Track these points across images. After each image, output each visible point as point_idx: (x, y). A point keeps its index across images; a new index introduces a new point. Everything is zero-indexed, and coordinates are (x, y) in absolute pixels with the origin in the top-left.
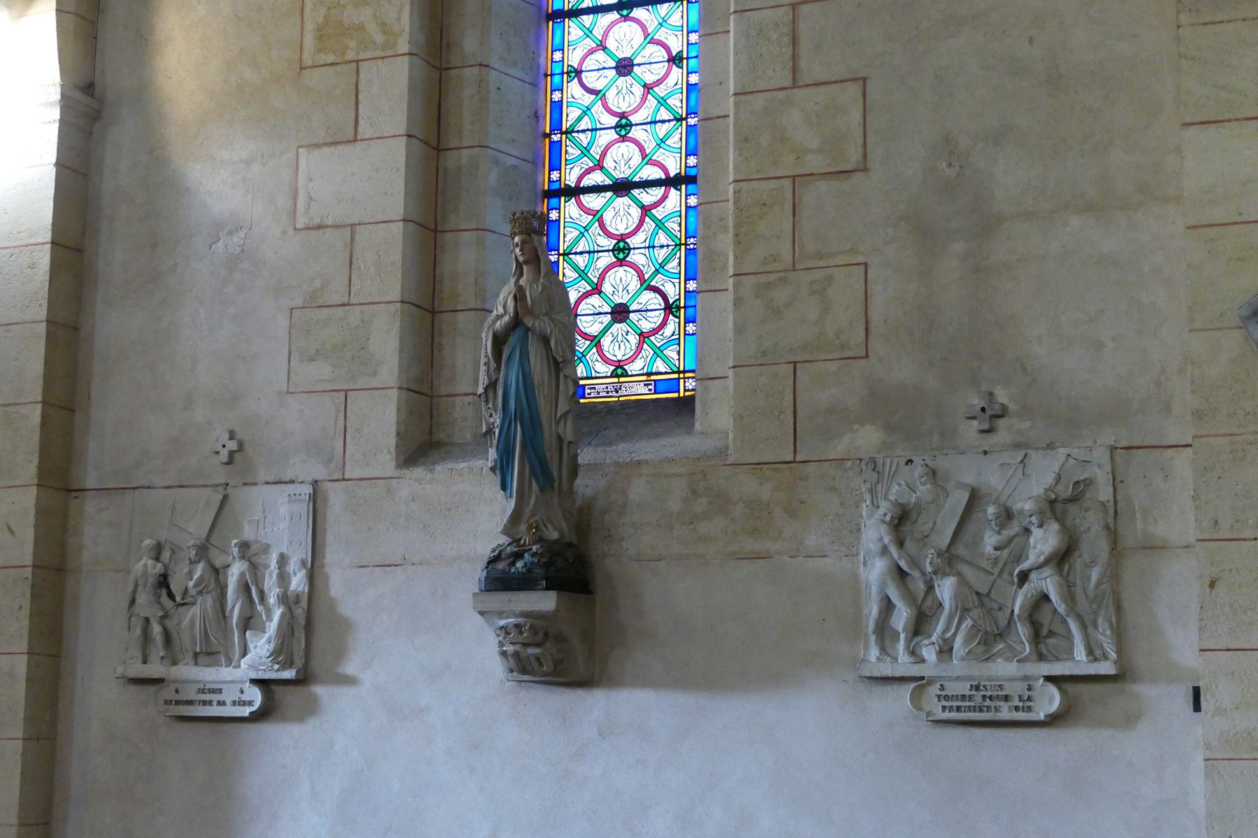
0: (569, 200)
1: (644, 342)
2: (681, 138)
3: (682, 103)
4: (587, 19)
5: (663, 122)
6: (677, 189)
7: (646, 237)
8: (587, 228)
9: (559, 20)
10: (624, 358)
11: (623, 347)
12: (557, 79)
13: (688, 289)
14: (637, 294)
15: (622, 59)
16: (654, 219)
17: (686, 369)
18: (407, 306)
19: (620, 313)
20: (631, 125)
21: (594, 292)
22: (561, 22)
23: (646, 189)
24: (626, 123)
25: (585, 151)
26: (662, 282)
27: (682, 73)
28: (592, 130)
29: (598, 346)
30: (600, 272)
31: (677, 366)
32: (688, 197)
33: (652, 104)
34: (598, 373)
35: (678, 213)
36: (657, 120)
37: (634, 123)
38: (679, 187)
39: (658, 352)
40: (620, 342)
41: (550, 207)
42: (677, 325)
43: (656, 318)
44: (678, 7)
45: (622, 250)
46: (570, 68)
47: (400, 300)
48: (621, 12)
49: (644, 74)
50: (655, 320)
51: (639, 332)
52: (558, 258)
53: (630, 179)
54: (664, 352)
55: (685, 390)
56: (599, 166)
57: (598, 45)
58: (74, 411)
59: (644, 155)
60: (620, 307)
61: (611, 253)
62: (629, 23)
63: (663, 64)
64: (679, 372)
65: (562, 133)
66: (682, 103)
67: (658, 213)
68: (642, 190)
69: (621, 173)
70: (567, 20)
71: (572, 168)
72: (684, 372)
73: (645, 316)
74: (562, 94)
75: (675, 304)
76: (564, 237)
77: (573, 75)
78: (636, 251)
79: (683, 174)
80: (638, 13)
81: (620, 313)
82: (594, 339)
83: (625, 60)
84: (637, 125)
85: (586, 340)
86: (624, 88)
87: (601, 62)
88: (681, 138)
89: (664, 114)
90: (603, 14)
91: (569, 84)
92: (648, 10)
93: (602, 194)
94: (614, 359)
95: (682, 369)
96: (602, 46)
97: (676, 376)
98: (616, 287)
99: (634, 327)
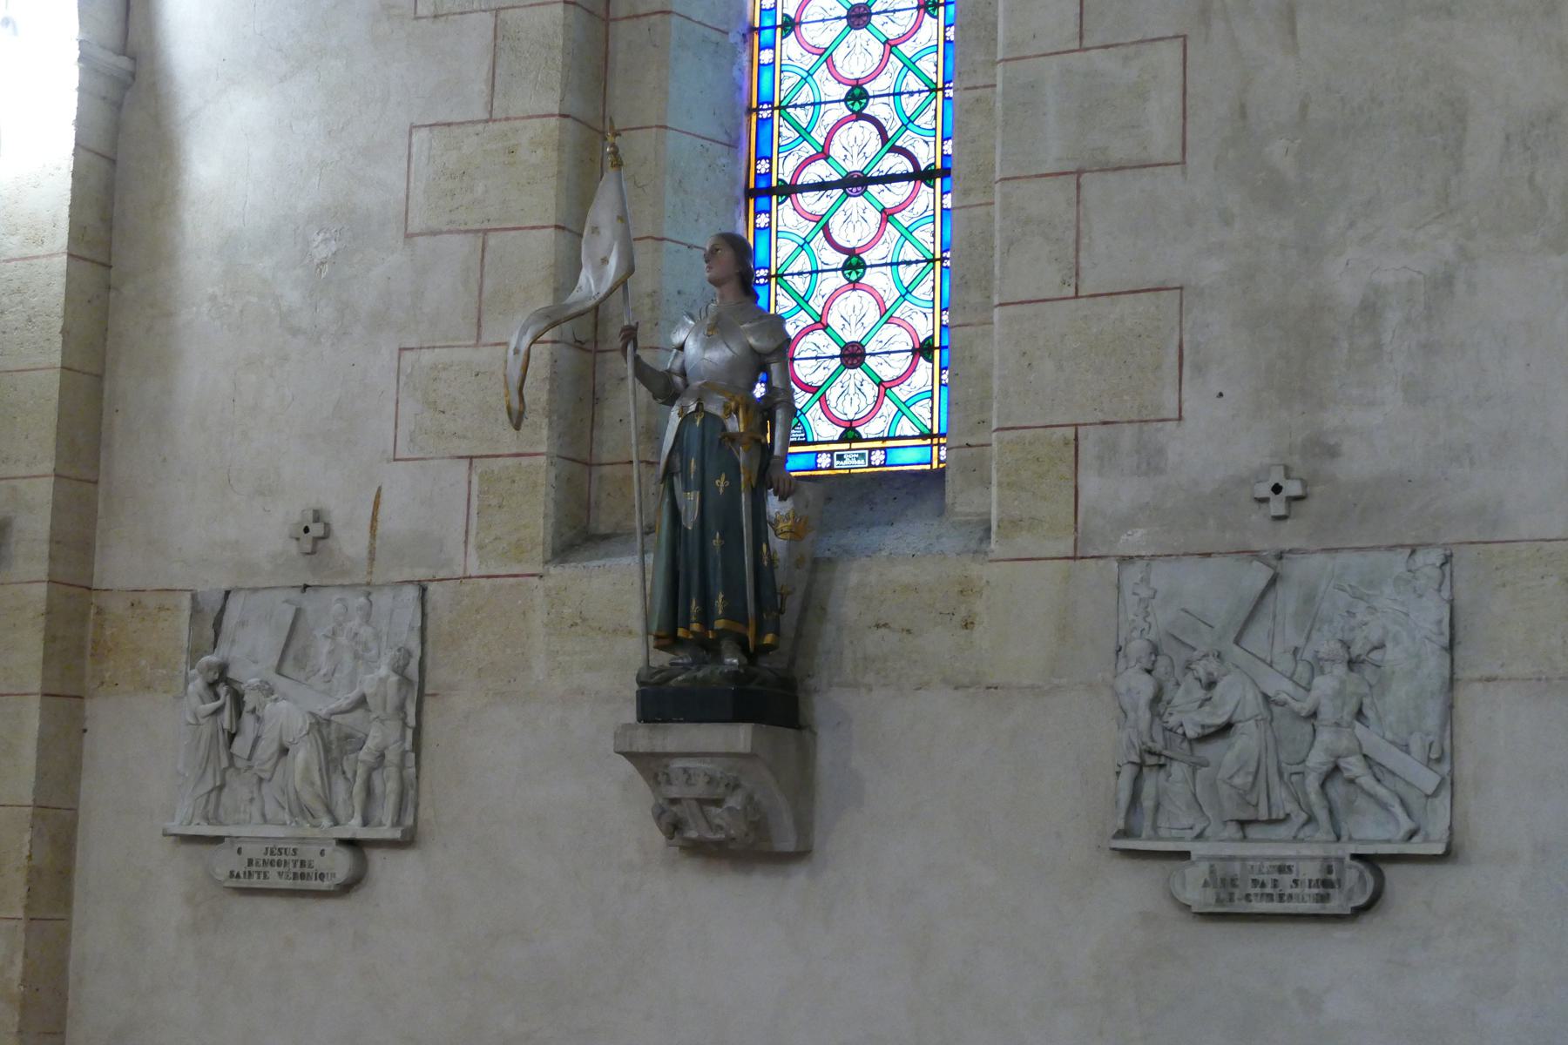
1: (885, 395)
2: (934, 288)
5: (909, 263)
6: (929, 186)
10: (857, 417)
11: (855, 402)
12: (767, 34)
13: (948, 39)
15: (849, 343)
18: (568, 122)
19: (853, 355)
21: (819, 156)
23: (888, 185)
24: (861, 94)
25: (804, 134)
28: (813, 104)
29: (823, 401)
30: (828, 130)
34: (827, 264)
35: (929, 394)
36: (900, 261)
38: (930, 358)
39: (903, 409)
40: (852, 396)
41: (759, 208)
43: (901, 363)
47: (553, 222)
51: (884, 39)
52: (772, 113)
53: (865, 172)
55: (940, 462)
56: (824, 154)
58: (111, 267)
59: (883, 311)
60: (860, 8)
62: (862, 123)
63: (911, 11)
65: (773, 109)
67: (903, 218)
69: (855, 165)
71: (786, 157)
73: (892, 18)
74: (771, 163)
76: (781, 84)
78: (877, 100)
81: (853, 355)
82: (817, 391)
83: (853, 346)
85: (807, 392)
86: (853, 324)
88: (934, 288)
89: (910, 253)
91: (780, 207)
93: (829, 192)
98: (848, 319)
99: (871, 374)
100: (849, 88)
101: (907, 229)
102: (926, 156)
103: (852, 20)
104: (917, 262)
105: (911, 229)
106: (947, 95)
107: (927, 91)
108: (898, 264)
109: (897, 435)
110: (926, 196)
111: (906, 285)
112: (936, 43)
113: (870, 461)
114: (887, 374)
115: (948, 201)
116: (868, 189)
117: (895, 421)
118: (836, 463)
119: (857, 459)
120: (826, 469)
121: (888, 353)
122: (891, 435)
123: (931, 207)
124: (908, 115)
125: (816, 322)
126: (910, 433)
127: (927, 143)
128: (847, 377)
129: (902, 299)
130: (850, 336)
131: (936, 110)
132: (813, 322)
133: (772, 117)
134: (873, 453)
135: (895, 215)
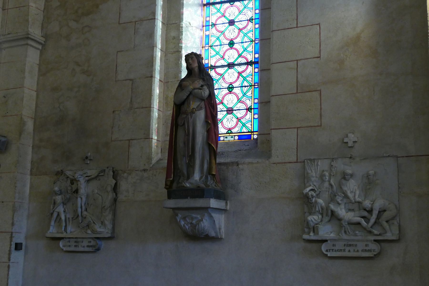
0: (212, 70)
3: (253, 35)
4: (218, 6)
5: (245, 86)
6: (251, 66)
7: (238, 129)
8: (219, 37)
9: (208, 6)
14: (236, 104)
15: (233, 25)
16: (243, 77)
17: (254, 131)
20: (234, 87)
22: (209, 7)
23: (240, 66)
24: (232, 87)
26: (245, 100)
27: (252, 68)
29: (224, 34)
31: (251, 130)
32: (255, 115)
33: (242, 35)
36: (243, 86)
37: (234, 86)
40: (230, 121)
42: (251, 115)
44: (250, 40)
45: (231, 88)
46: (212, 23)
48: (230, 3)
49: (239, 25)
50: (243, 113)
54: (246, 125)
57: (220, 102)
61: (228, 45)
64: (251, 132)
66: (253, 35)
67: (244, 74)
68: (238, 66)
69: (231, 61)
70: (211, 6)
72: (253, 132)
75: (251, 18)
77: (213, 26)
79: (253, 61)
80: (237, 3)
84: (235, 87)
86: (230, 119)
87: (222, 109)
90: (224, 4)
92: (240, 2)
94: (228, 127)
95: (252, 131)
96: (224, 16)
97: (250, 133)
98: (230, 14)
99: (235, 116)
100: (230, 41)
101: (245, 33)
102: (250, 58)
103: (228, 112)
104: (248, 86)
105: (246, 77)
106: (256, 42)
107: (250, 42)
108: (242, 87)
109: (242, 132)
110: (250, 68)
111: (244, 92)
112: (252, 29)
113: (234, 138)
114: (239, 116)
115: (257, 70)
116: (235, 24)
117: (241, 128)
118: (225, 139)
119: (231, 138)
120: (223, 141)
121: (241, 21)
122: (241, 132)
123: (251, 71)
124: (246, 5)
125: (222, 15)
126: (246, 131)
127: (249, 100)
128: (228, 117)
129: (243, 96)
130: (231, 18)
131: (253, 46)
132: (219, 102)
133: (209, 49)
134: (235, 136)
135: (242, 74)
